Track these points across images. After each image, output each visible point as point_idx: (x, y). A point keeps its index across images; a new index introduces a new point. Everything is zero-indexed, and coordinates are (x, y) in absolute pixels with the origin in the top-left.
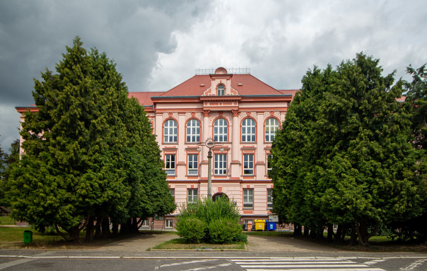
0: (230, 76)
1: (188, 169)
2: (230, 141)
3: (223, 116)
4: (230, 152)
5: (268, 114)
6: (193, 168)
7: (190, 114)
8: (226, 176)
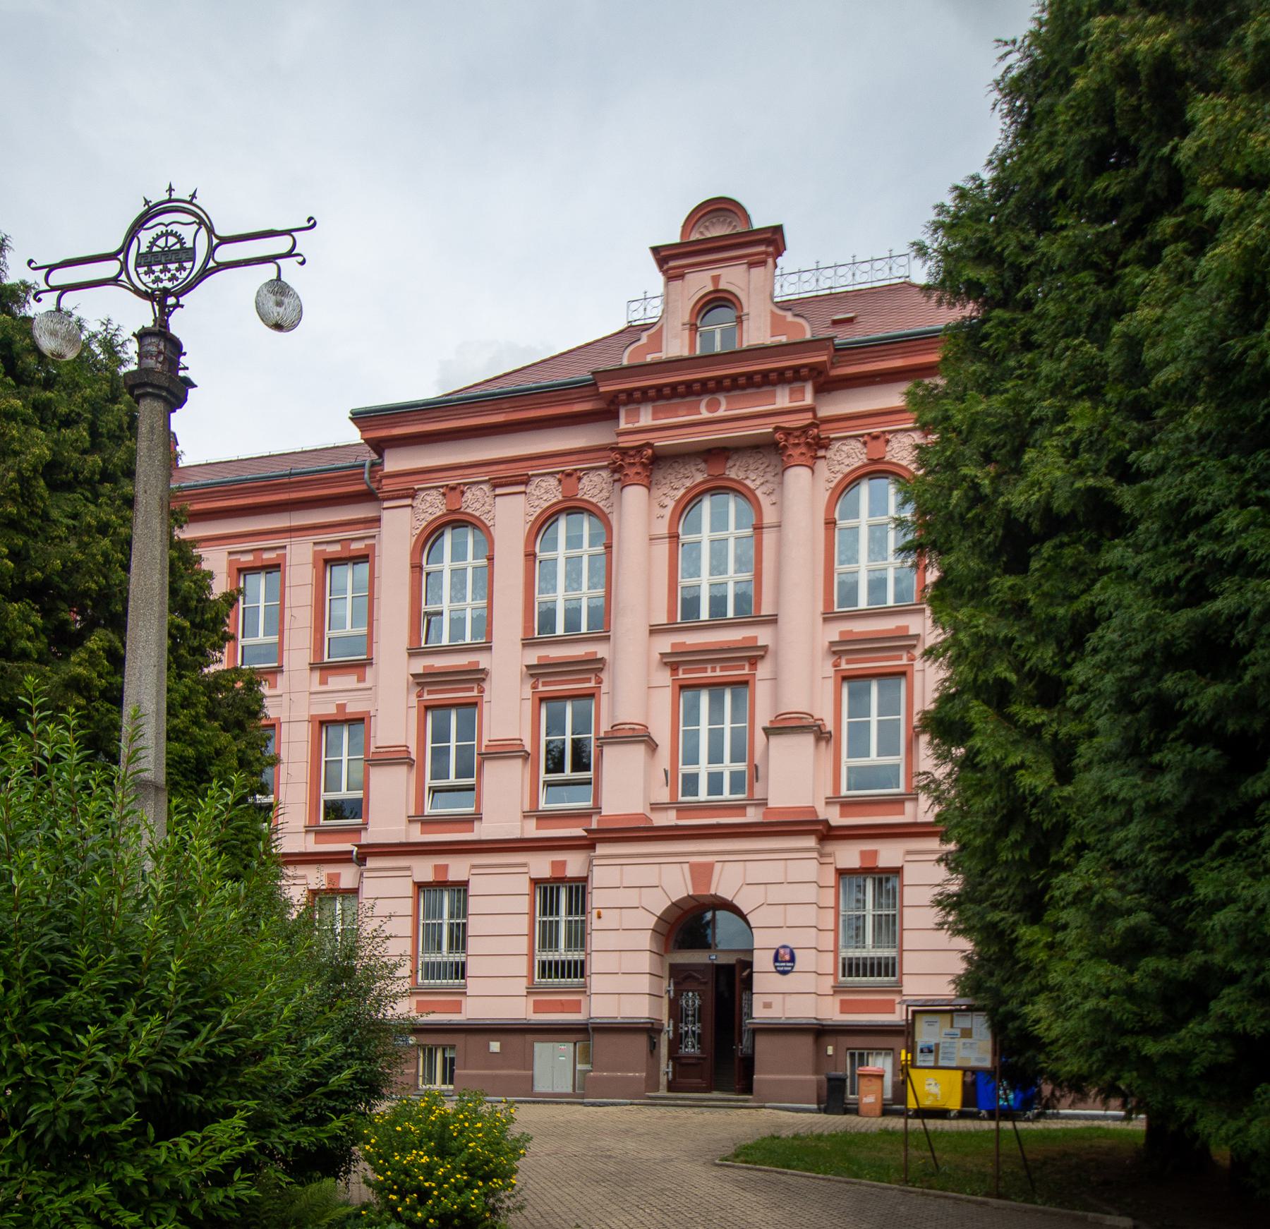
0: (768, 242)
1: (543, 776)
2: (766, 610)
3: (732, 474)
4: (763, 670)
5: (547, 492)
6: (568, 774)
7: (553, 482)
8: (744, 807)
